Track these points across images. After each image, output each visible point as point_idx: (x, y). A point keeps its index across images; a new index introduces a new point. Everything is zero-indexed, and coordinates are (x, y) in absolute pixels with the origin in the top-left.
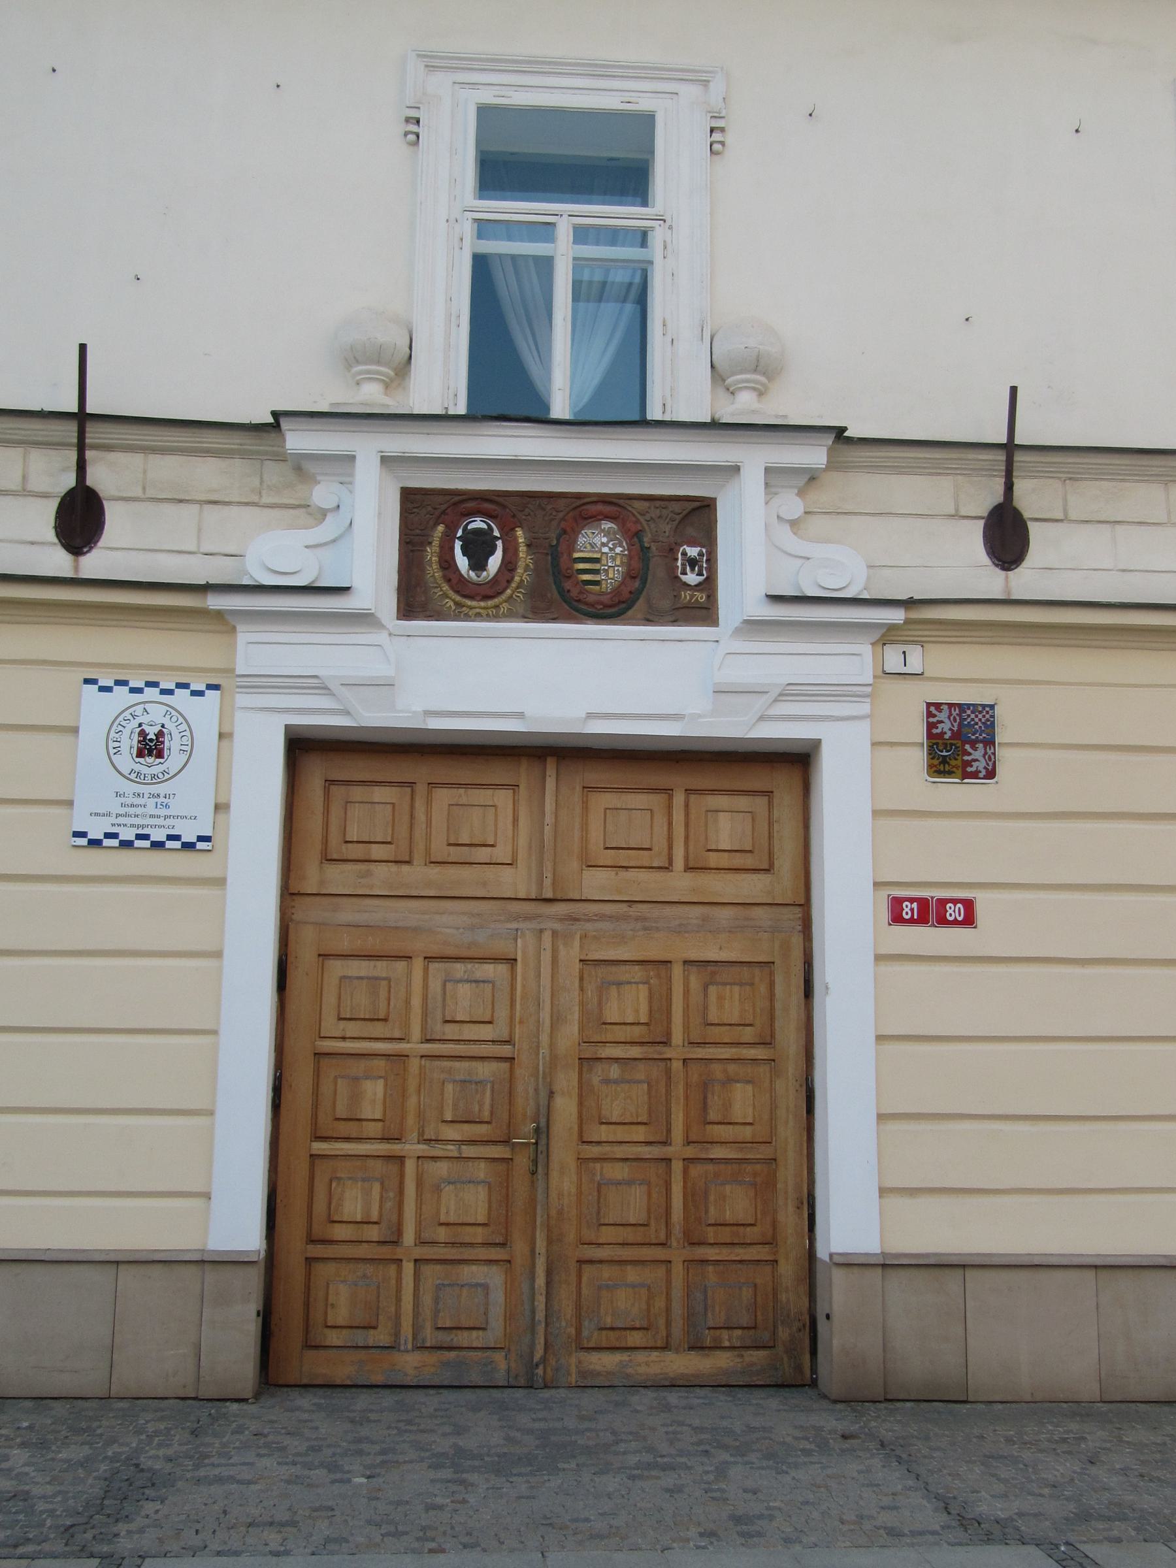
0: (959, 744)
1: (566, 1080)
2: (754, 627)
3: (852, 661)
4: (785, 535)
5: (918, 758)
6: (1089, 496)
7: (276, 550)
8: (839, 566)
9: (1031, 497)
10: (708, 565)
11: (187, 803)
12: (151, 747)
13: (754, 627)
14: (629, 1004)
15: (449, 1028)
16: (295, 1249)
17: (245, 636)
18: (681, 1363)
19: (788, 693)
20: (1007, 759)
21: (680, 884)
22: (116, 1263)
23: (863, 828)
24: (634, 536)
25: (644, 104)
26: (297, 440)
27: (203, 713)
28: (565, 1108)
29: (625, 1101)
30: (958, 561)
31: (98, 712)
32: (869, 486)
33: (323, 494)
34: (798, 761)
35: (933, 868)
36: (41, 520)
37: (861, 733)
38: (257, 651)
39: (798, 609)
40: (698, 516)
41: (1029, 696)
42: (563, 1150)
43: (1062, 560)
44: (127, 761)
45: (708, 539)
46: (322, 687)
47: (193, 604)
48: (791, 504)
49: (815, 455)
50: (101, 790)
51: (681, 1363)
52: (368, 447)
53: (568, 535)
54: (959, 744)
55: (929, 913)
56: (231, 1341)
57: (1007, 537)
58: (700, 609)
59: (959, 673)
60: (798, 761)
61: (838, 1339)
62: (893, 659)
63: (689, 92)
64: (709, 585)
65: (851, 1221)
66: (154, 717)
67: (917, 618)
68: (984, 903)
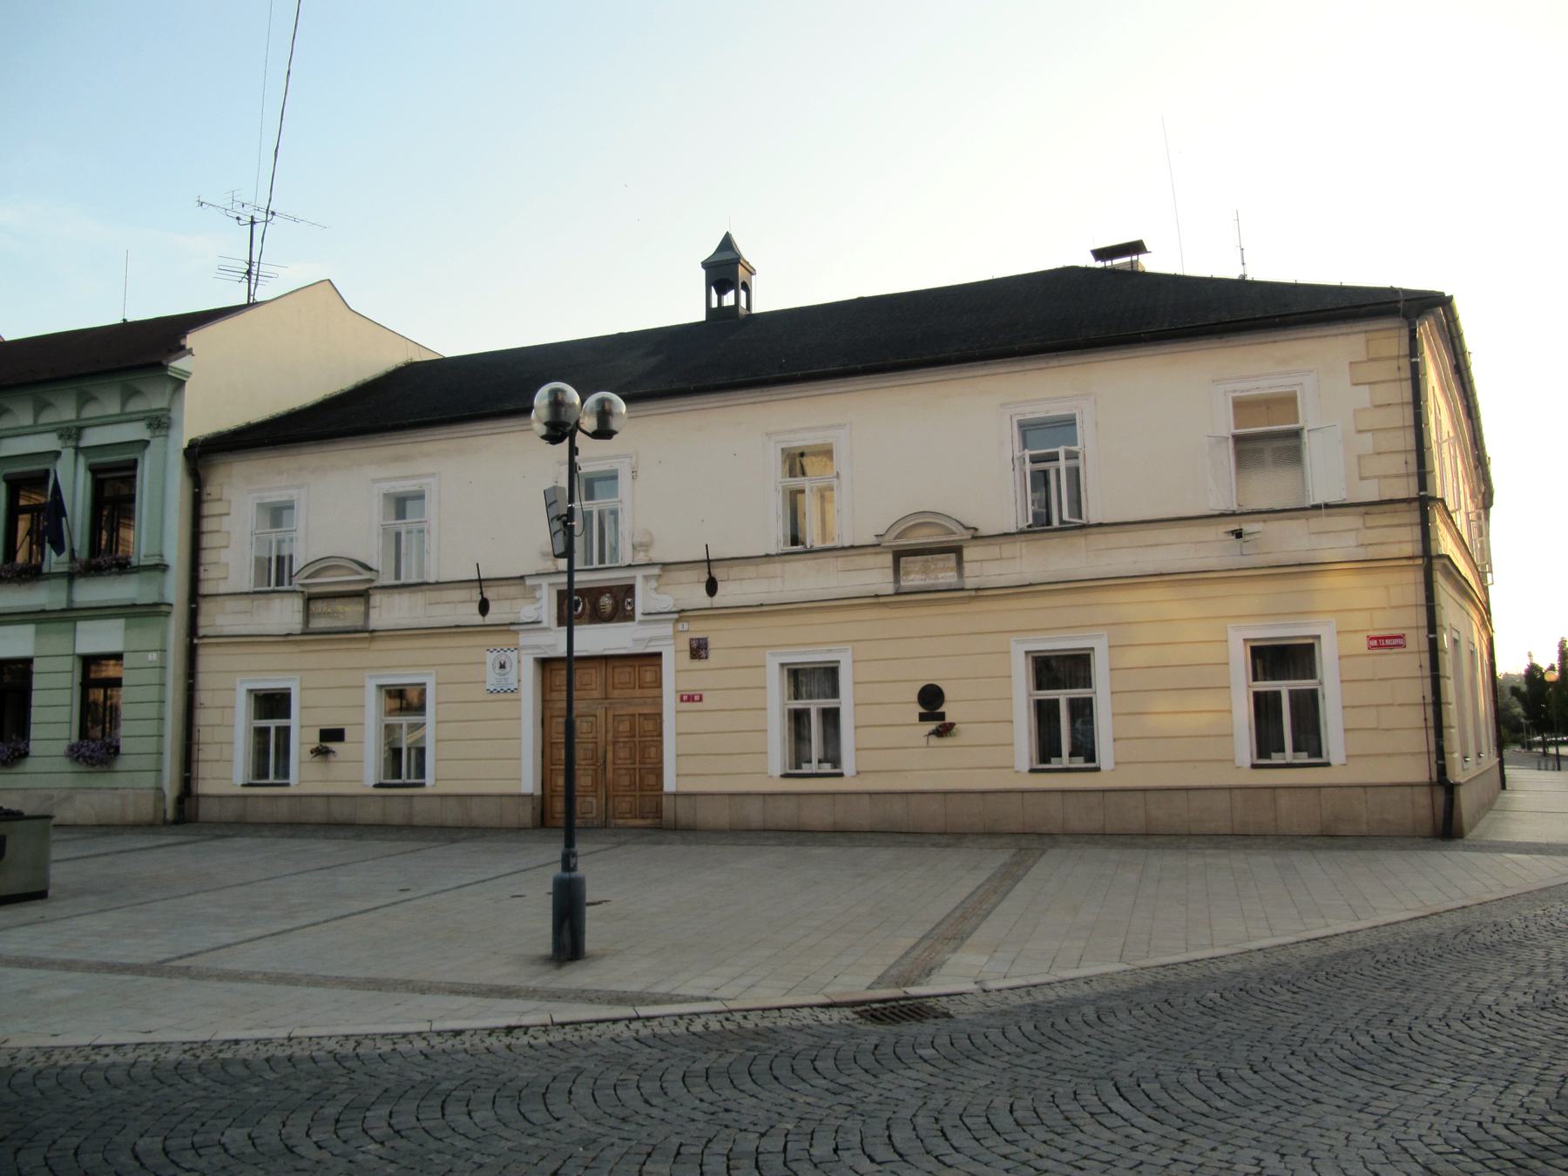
0: (698, 650)
1: (610, 748)
2: (641, 622)
3: (667, 629)
4: (654, 595)
5: (688, 654)
6: (736, 571)
7: (527, 612)
8: (666, 602)
9: (718, 573)
10: (632, 604)
11: (511, 679)
12: (502, 666)
13: (641, 622)
14: (624, 727)
15: (132, 732)
16: (548, 791)
17: (521, 635)
18: (638, 822)
19: (651, 639)
20: (712, 654)
21: (638, 692)
22: (501, 796)
23: (674, 673)
24: (614, 597)
25: (616, 466)
26: (529, 582)
27: (513, 656)
28: (610, 755)
29: (624, 753)
30: (696, 596)
31: (491, 658)
32: (676, 575)
33: (538, 594)
34: (659, 655)
35: (691, 685)
36: (475, 608)
37: (672, 649)
38: (525, 639)
39: (653, 616)
40: (629, 590)
41: (719, 635)
42: (610, 767)
43: (729, 593)
44: (498, 670)
45: (633, 596)
46: (538, 647)
47: (508, 628)
48: (653, 584)
49: (656, 571)
50: (492, 678)
51: (638, 822)
52: (544, 582)
53: (597, 600)
54: (698, 650)
55: (691, 699)
56: (526, 815)
57: (712, 587)
58: (630, 617)
59: (698, 629)
60: (659, 655)
61: (667, 813)
62: (680, 626)
63: (627, 461)
64: (633, 610)
65: (670, 785)
66: (503, 658)
67: (682, 614)
68: (706, 695)
